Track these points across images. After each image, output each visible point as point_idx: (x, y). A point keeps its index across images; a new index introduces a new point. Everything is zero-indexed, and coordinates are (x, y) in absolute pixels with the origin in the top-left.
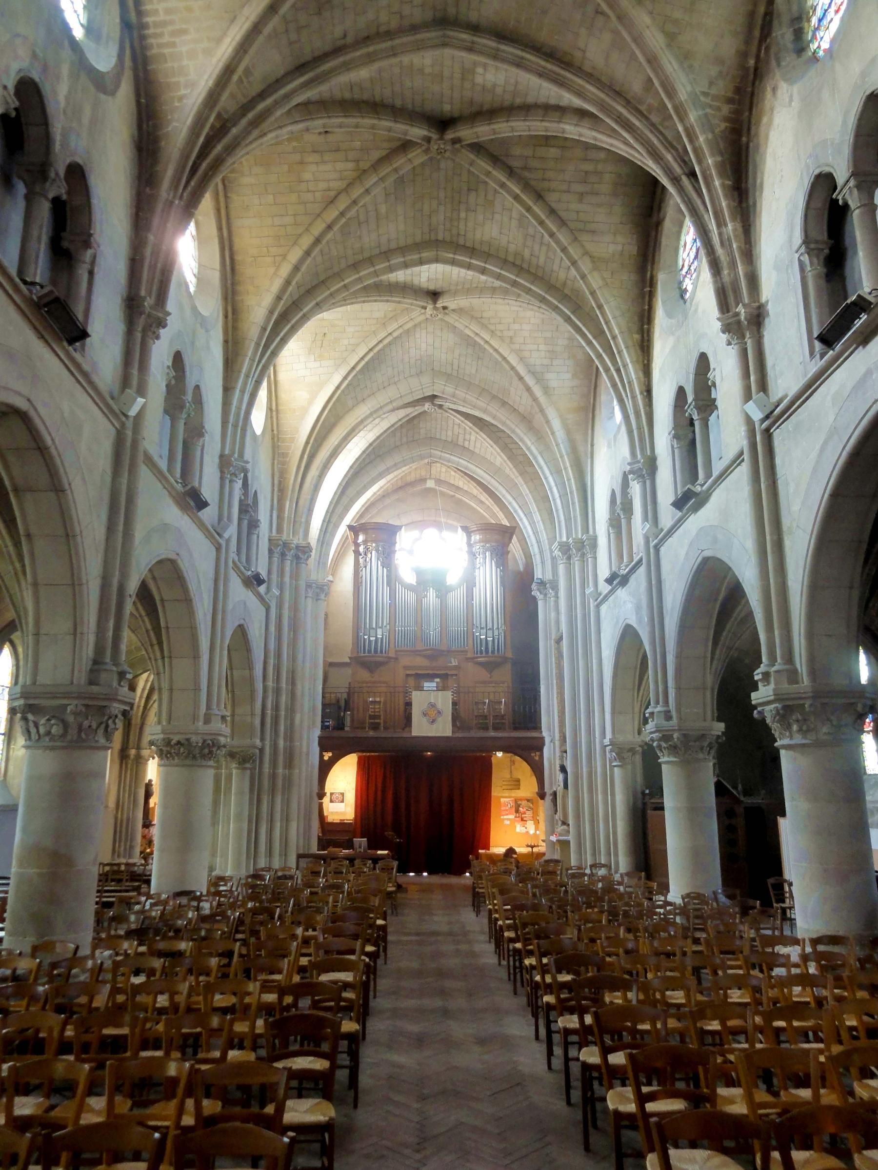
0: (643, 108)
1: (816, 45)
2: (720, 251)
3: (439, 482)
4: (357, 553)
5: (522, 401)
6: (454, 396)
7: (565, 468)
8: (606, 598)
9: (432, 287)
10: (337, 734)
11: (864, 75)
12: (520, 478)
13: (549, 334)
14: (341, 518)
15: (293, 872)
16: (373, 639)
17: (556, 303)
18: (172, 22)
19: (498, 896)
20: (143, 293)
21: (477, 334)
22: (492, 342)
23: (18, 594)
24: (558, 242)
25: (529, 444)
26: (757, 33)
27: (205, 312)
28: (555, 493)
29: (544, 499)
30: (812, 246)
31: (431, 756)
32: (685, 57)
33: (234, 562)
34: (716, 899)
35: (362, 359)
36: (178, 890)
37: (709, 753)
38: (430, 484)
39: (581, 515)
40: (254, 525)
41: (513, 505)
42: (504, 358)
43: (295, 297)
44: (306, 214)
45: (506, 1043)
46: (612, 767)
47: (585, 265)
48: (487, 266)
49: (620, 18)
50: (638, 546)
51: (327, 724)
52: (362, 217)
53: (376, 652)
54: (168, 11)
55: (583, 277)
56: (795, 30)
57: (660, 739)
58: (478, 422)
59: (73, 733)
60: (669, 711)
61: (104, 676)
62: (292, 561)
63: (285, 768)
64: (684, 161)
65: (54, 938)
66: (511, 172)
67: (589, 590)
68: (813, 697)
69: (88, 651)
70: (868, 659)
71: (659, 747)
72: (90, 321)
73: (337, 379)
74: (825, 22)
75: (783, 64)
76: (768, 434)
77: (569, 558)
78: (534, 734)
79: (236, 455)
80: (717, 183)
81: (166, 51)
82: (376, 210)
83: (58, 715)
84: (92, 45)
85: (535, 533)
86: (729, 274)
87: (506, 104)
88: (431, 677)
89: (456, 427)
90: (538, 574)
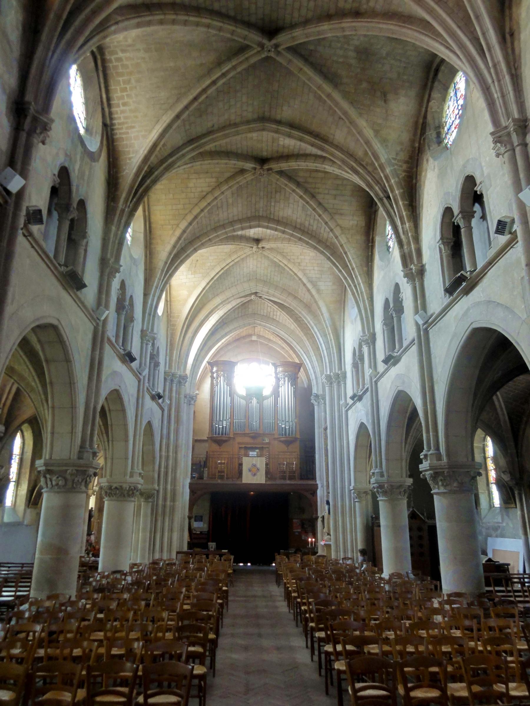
0: (364, 163)
1: (447, 141)
2: (403, 237)
3: (259, 336)
4: (212, 378)
5: (307, 298)
6: (268, 293)
7: (329, 334)
8: (351, 407)
9: (256, 237)
10: (200, 481)
11: (464, 166)
12: (304, 337)
13: (320, 262)
14: (204, 358)
15: (174, 561)
16: (221, 427)
17: (322, 249)
18: (126, 123)
19: (289, 574)
20: (109, 256)
21: (280, 261)
22: (289, 265)
23: (42, 412)
24: (323, 219)
25: (308, 319)
26: (419, 132)
27: (135, 256)
28: (323, 347)
29: (317, 349)
30: (445, 241)
31: (253, 495)
32: (384, 141)
33: (147, 389)
34: (408, 577)
35: (217, 273)
36: (114, 570)
37: (404, 495)
38: (254, 338)
39: (337, 360)
40: (157, 365)
41: (301, 352)
42: (295, 274)
43: (183, 245)
44: (190, 204)
45: (291, 649)
46: (355, 502)
47: (338, 231)
48: (286, 230)
49: (350, 123)
50: (367, 380)
51: (194, 475)
52: (219, 205)
53: (222, 434)
54: (125, 118)
55: (337, 237)
56: (437, 133)
57: (378, 488)
58: (281, 306)
59: (70, 484)
60: (383, 472)
61: (85, 455)
62: (176, 384)
63: (171, 501)
64: (385, 191)
65: (58, 592)
66: (298, 184)
67: (342, 402)
68: (448, 468)
69: (78, 441)
70: (493, 442)
71: (378, 492)
72: (84, 275)
73: (203, 284)
74: (450, 131)
75: (431, 148)
76: (426, 332)
77: (331, 383)
78: (311, 482)
79: (150, 330)
80: (401, 203)
81: (124, 136)
82: (227, 201)
83: (62, 474)
84: (88, 137)
85: (313, 368)
86: (407, 248)
87: (296, 153)
88: (253, 449)
89: (269, 308)
90: (315, 391)
